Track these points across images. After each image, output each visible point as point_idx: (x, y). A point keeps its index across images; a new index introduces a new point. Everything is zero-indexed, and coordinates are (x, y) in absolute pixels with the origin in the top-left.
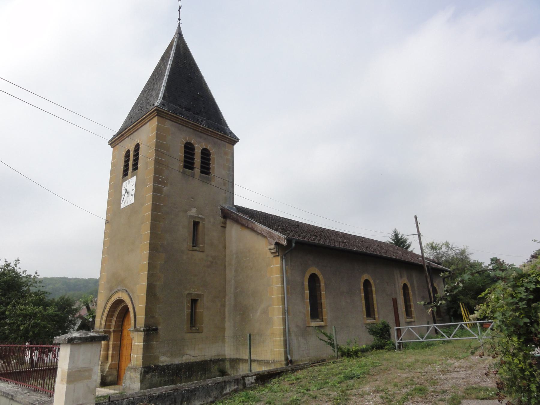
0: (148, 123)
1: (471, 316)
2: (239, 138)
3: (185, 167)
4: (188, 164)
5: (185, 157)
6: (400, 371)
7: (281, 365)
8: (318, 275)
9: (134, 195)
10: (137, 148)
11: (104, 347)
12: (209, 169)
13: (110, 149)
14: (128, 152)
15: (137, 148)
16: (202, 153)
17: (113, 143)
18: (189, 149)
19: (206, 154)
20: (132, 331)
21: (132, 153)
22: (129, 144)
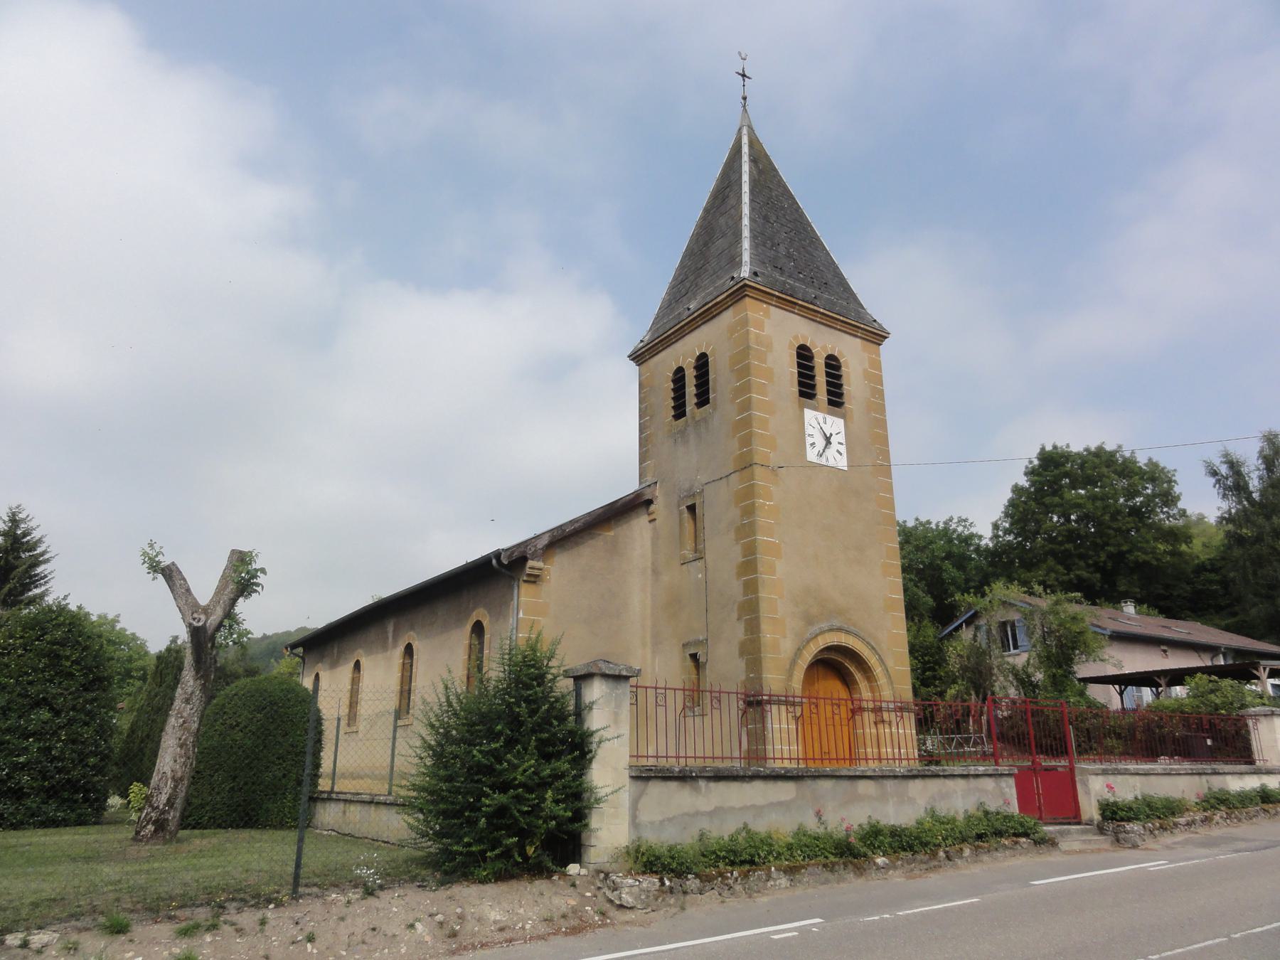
0: (731, 308)
1: (1014, 616)
2: (889, 330)
3: (802, 394)
4: (806, 390)
5: (800, 374)
6: (1228, 695)
7: (1262, 719)
8: (486, 632)
9: (808, 446)
10: (702, 363)
11: (1146, 762)
12: (840, 395)
13: (633, 368)
14: (680, 371)
15: (702, 363)
16: (827, 365)
17: (640, 357)
18: (804, 355)
19: (833, 364)
20: (851, 730)
21: (690, 375)
22: (683, 353)
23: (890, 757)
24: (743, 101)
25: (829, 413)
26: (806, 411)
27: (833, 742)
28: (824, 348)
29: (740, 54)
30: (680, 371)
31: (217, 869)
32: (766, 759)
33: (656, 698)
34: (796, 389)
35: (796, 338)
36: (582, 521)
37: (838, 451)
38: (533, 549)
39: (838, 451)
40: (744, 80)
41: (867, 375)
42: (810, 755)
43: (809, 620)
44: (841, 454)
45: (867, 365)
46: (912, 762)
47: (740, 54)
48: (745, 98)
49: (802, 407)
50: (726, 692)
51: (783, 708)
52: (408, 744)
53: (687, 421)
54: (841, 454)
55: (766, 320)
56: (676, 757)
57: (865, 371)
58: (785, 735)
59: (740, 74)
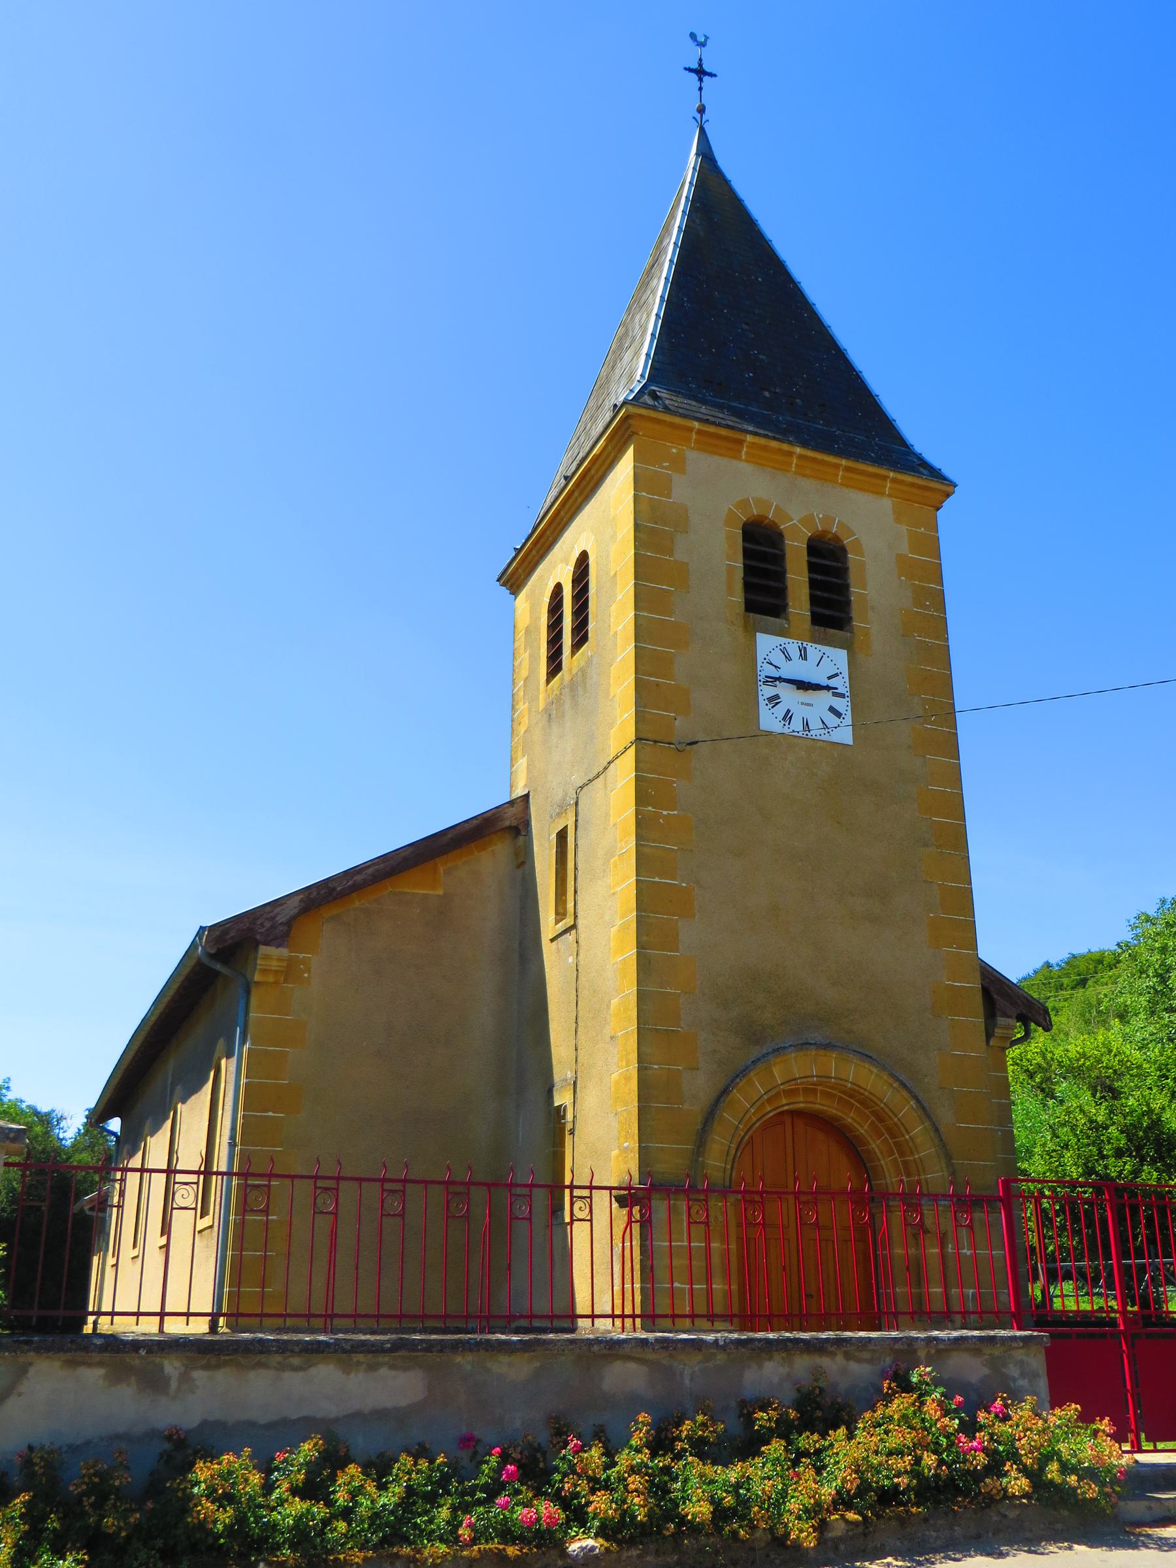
5: (748, 570)
9: (762, 703)
10: (582, 564)
14: (558, 588)
23: (701, 1309)
24: (698, 116)
25: (815, 640)
26: (760, 637)
27: (615, 1276)
28: (808, 520)
29: (693, 36)
30: (558, 588)
31: (1022, 1362)
32: (574, 1317)
33: (315, 1199)
34: (738, 598)
35: (744, 504)
36: (370, 871)
37: (832, 709)
38: (268, 925)
39: (832, 709)
40: (701, 80)
41: (905, 566)
42: (663, 1307)
43: (752, 1034)
44: (838, 714)
45: (904, 548)
46: (1058, 1292)
47: (693, 36)
48: (702, 110)
49: (751, 631)
50: (338, 1186)
51: (891, 1191)
52: (827, 1246)
53: (563, 675)
54: (838, 714)
55: (676, 478)
56: (325, 1316)
57: (901, 559)
58: (680, 1262)
59: (690, 70)
